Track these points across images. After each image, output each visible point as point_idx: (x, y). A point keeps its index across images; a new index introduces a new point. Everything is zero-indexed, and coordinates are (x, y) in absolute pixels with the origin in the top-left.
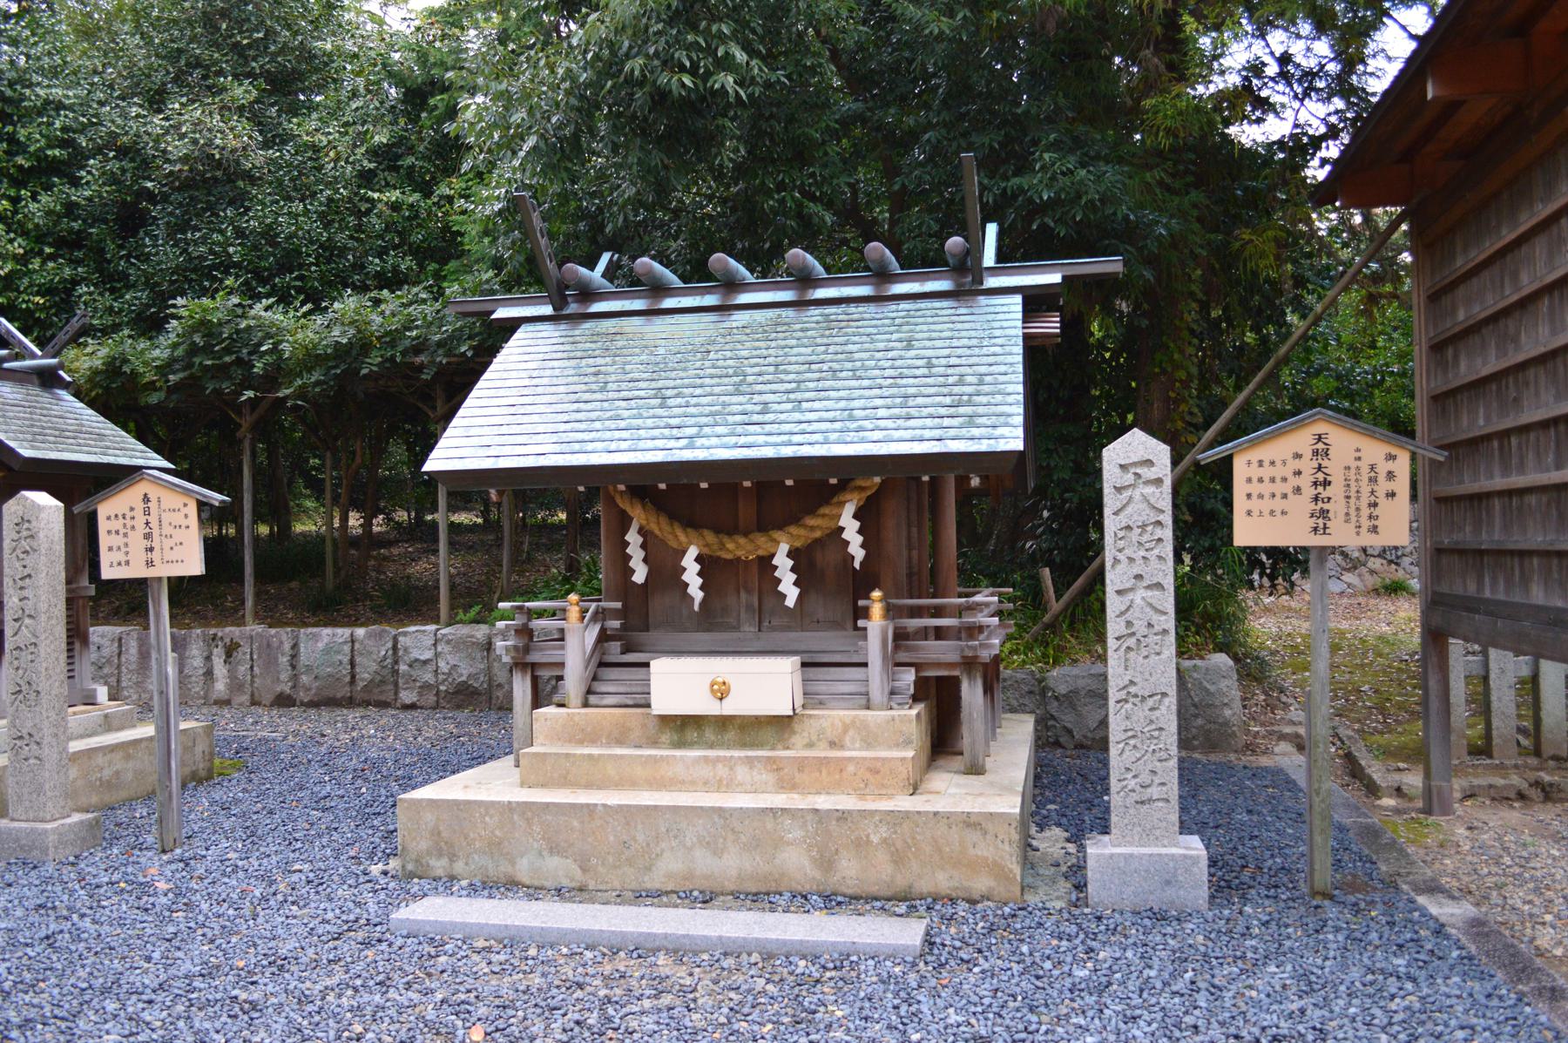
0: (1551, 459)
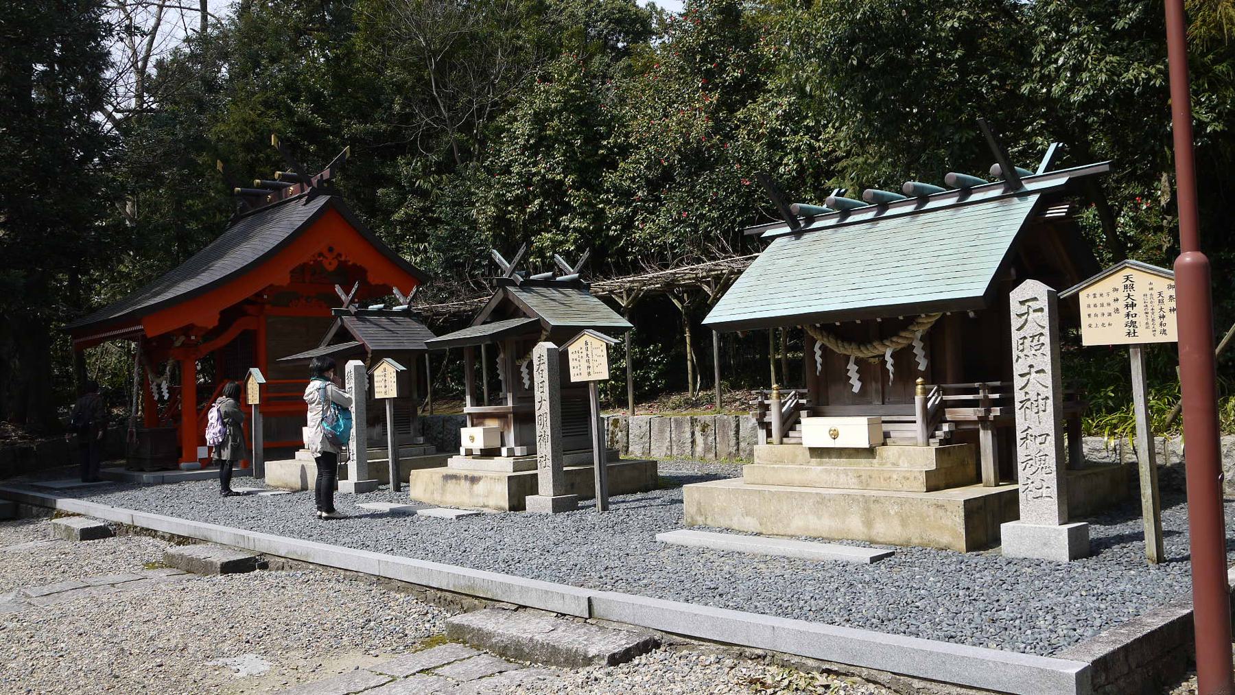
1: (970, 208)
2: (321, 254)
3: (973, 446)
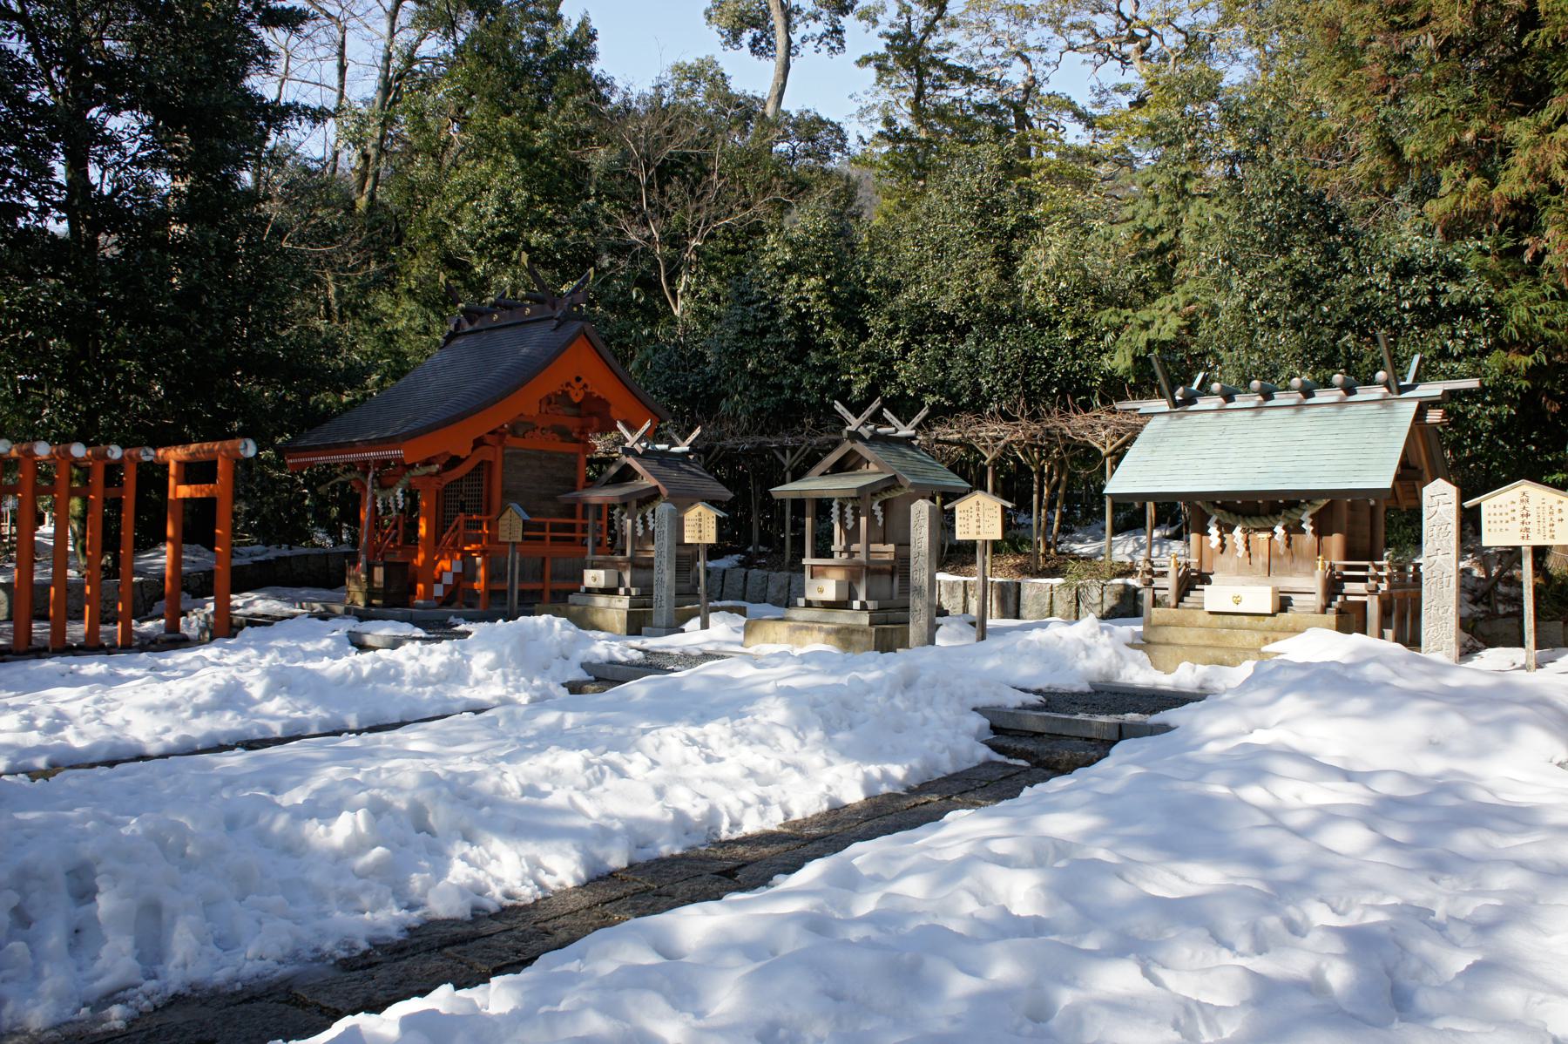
0: (782, 1033)
1: (1354, 407)
2: (568, 384)
3: (1516, 621)
